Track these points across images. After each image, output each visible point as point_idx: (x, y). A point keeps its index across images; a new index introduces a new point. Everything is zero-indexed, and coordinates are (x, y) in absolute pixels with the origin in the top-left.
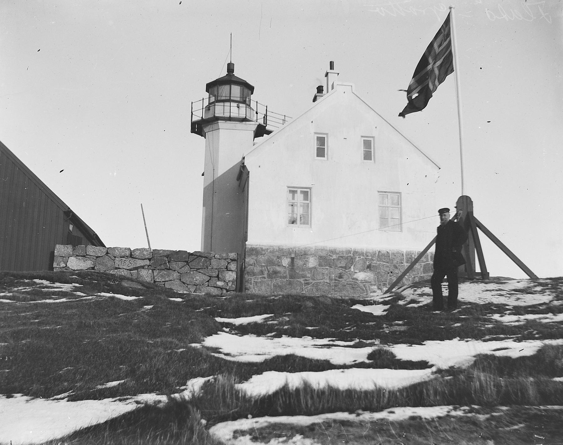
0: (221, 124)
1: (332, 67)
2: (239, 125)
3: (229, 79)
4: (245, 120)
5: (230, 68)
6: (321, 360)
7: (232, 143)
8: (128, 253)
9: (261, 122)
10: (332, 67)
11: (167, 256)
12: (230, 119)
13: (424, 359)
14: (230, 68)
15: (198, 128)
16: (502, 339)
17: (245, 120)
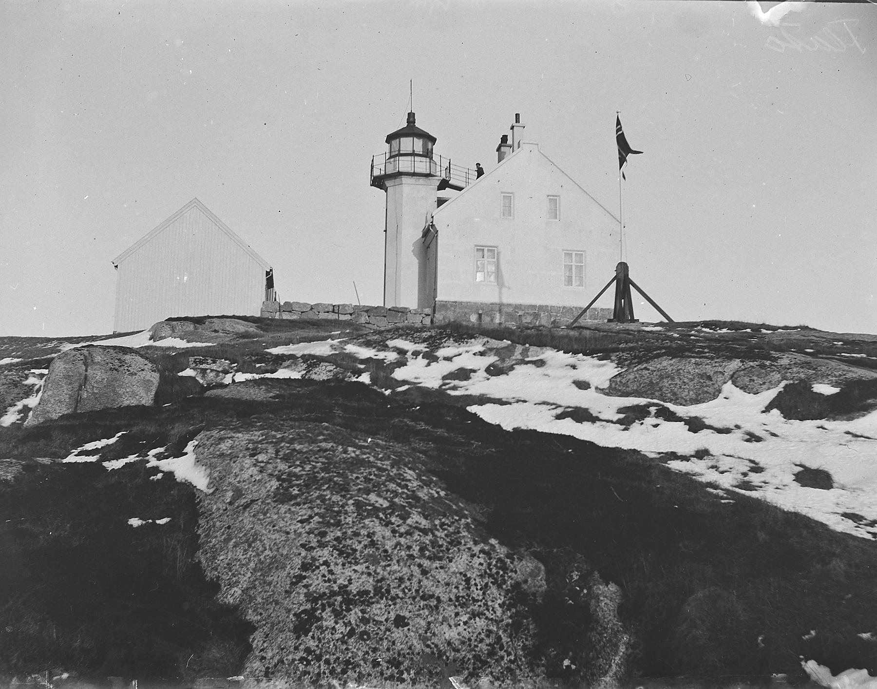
0: (405, 180)
1: (517, 120)
2: (422, 180)
3: (411, 130)
4: (428, 175)
5: (411, 117)
6: (486, 304)
7: (415, 197)
8: (331, 309)
9: (443, 176)
10: (517, 120)
11: (367, 311)
12: (414, 174)
13: (831, 472)
14: (411, 117)
15: (379, 182)
16: (309, 340)
17: (428, 175)
